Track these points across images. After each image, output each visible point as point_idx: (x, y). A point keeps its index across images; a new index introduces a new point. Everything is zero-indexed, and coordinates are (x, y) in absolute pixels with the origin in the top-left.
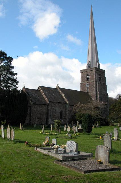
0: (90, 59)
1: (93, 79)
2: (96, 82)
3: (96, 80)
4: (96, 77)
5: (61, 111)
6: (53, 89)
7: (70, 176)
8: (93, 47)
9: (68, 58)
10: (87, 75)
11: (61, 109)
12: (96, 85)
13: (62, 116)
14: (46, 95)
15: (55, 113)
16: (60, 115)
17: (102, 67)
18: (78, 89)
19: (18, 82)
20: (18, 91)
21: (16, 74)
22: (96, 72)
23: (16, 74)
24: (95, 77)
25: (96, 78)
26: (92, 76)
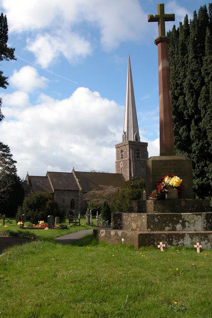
0: (126, 131)
1: (126, 157)
2: (130, 160)
3: (130, 158)
4: (130, 153)
5: (72, 199)
6: (65, 175)
7: (69, 269)
8: (129, 113)
9: (164, 107)
10: (122, 151)
11: (72, 198)
12: (130, 164)
13: (74, 205)
14: (52, 183)
15: (64, 202)
16: (71, 204)
17: (143, 140)
18: (113, 171)
19: (12, 57)
20: (16, 178)
21: (16, 162)
22: (130, 148)
23: (16, 162)
24: (128, 154)
25: (130, 155)
26: (126, 153)
